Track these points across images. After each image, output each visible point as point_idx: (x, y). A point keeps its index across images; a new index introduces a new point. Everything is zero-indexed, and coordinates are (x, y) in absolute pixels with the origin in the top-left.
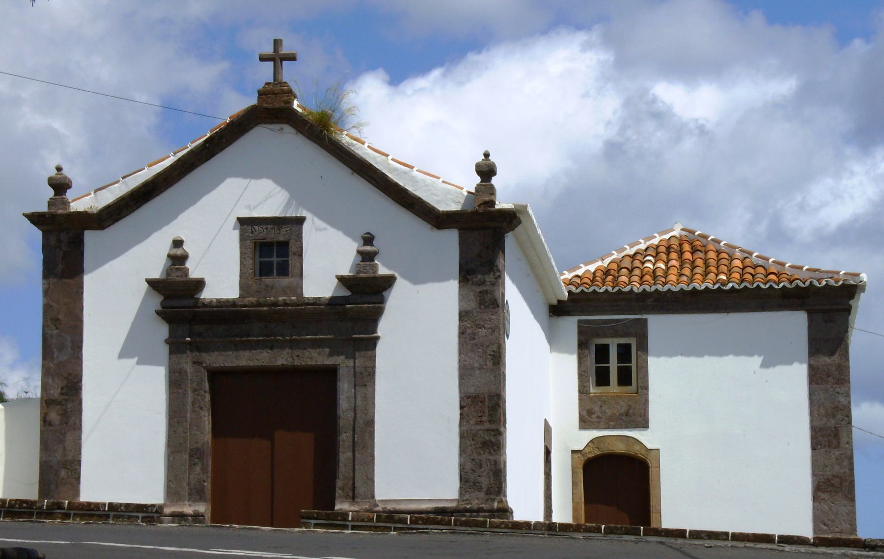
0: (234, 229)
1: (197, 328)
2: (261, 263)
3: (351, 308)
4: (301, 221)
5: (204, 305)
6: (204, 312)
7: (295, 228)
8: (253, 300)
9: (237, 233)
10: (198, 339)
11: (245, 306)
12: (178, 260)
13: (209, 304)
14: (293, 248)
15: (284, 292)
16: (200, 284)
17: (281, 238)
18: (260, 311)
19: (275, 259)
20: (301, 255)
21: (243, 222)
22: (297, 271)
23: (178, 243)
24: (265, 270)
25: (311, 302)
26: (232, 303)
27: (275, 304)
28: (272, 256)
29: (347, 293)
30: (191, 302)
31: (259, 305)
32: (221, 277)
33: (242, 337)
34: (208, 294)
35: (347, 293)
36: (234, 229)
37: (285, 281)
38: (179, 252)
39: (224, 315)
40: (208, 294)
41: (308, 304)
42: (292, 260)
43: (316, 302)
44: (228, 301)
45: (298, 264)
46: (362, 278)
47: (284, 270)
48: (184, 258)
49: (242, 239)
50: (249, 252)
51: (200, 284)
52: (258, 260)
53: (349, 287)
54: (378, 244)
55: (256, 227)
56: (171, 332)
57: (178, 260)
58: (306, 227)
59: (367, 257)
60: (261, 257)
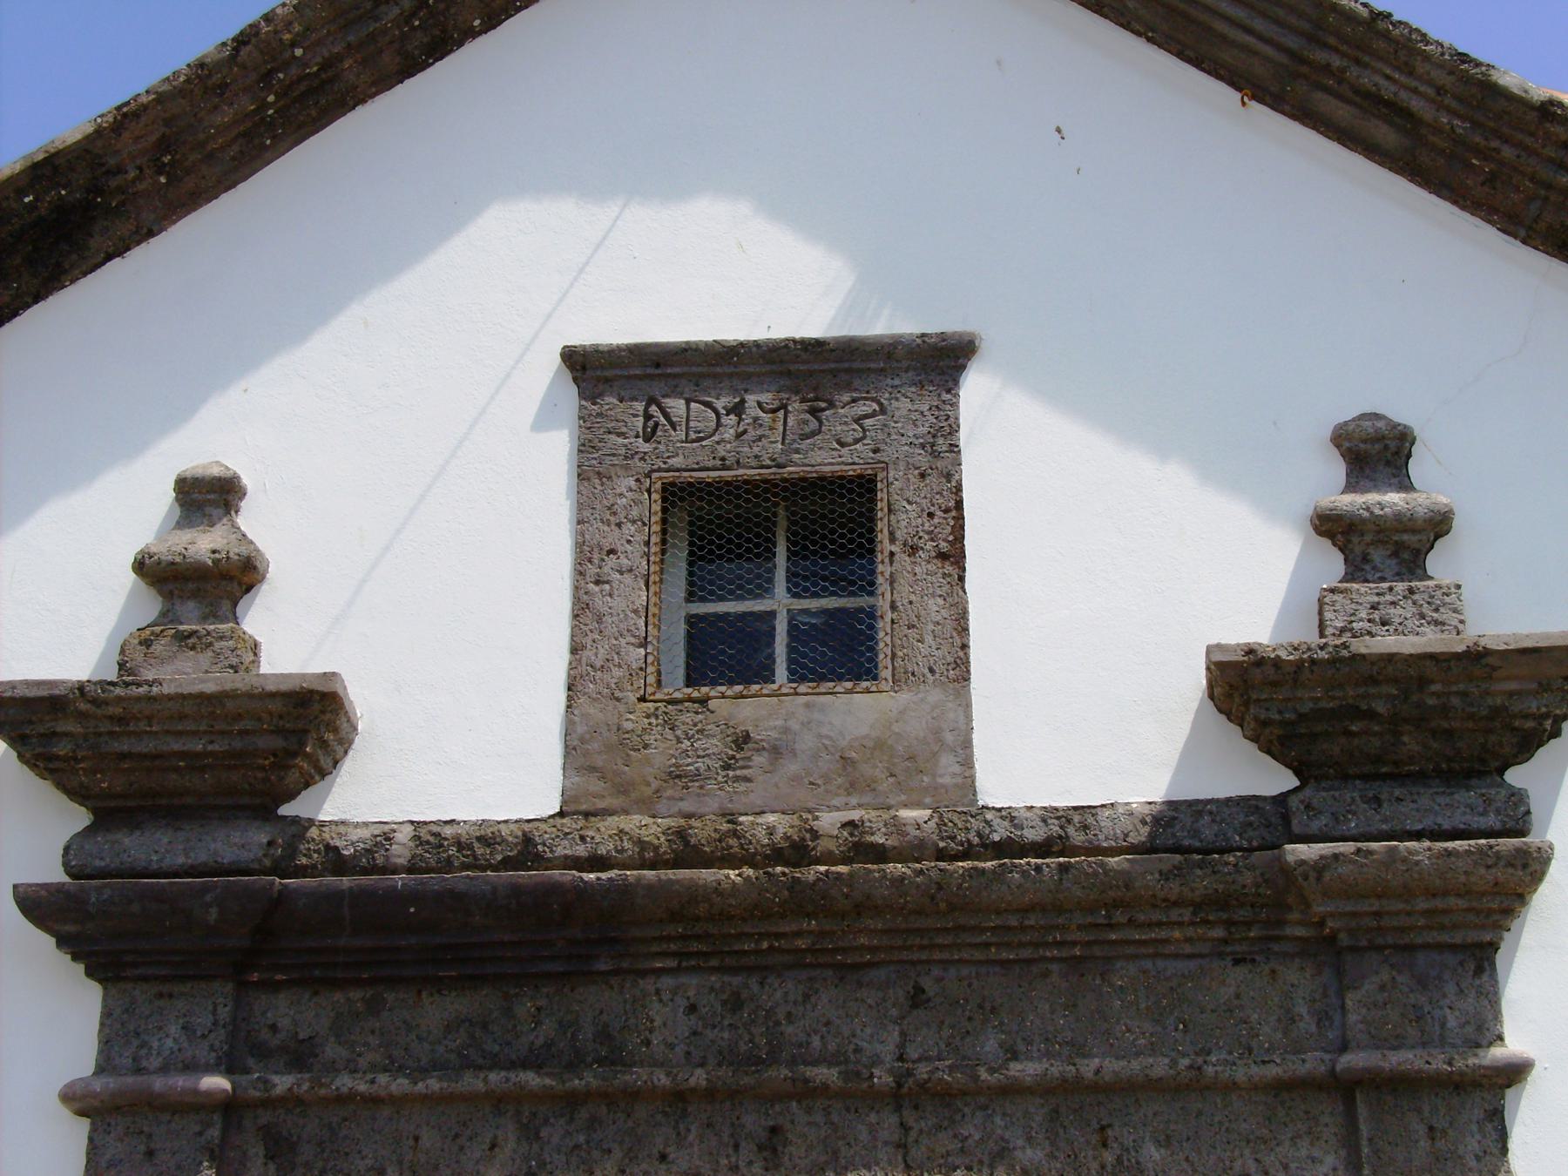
0: (542, 422)
1: (288, 1013)
2: (692, 621)
3: (1320, 867)
4: (941, 361)
5: (336, 861)
6: (336, 896)
7: (908, 406)
8: (649, 827)
9: (557, 450)
10: (283, 1083)
11: (597, 862)
12: (199, 585)
13: (372, 856)
14: (902, 514)
15: (848, 768)
16: (309, 723)
17: (823, 459)
18: (694, 894)
19: (780, 601)
20: (954, 556)
21: (589, 369)
22: (929, 649)
23: (207, 496)
24: (722, 654)
25: (1033, 834)
26: (524, 847)
27: (798, 851)
28: (763, 588)
29: (1273, 780)
30: (241, 842)
31: (687, 853)
32: (459, 703)
33: (575, 1064)
34: (374, 793)
35: (1273, 780)
36: (542, 422)
37: (852, 713)
38: (204, 543)
39: (474, 922)
40: (374, 793)
41: (1009, 848)
42: (901, 583)
43: (1065, 834)
44: (488, 835)
45: (934, 607)
46: (1390, 658)
47: (842, 652)
48: (237, 577)
49: (591, 468)
50: (633, 544)
51: (309, 723)
52: (677, 609)
53: (1276, 739)
54: (1433, 480)
55: (677, 406)
56: (118, 1038)
57: (199, 585)
58: (976, 390)
59: (1380, 543)
60: (691, 597)
